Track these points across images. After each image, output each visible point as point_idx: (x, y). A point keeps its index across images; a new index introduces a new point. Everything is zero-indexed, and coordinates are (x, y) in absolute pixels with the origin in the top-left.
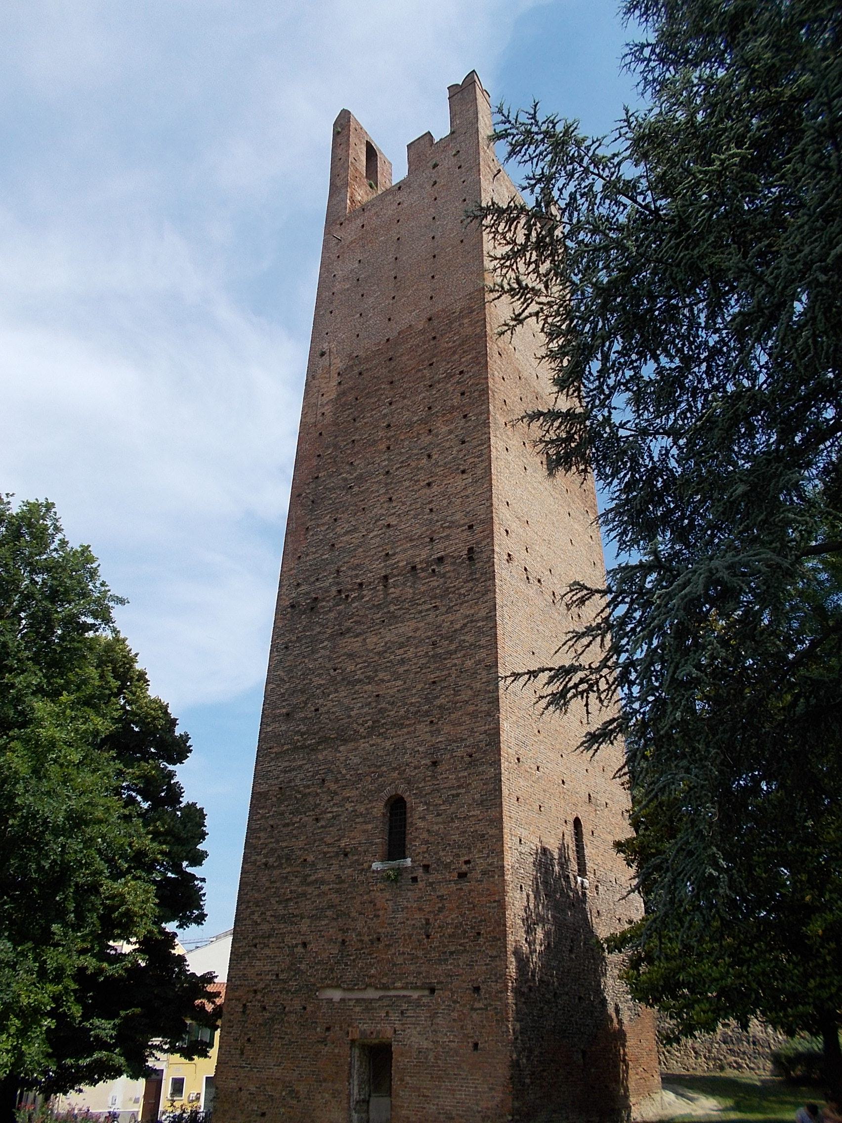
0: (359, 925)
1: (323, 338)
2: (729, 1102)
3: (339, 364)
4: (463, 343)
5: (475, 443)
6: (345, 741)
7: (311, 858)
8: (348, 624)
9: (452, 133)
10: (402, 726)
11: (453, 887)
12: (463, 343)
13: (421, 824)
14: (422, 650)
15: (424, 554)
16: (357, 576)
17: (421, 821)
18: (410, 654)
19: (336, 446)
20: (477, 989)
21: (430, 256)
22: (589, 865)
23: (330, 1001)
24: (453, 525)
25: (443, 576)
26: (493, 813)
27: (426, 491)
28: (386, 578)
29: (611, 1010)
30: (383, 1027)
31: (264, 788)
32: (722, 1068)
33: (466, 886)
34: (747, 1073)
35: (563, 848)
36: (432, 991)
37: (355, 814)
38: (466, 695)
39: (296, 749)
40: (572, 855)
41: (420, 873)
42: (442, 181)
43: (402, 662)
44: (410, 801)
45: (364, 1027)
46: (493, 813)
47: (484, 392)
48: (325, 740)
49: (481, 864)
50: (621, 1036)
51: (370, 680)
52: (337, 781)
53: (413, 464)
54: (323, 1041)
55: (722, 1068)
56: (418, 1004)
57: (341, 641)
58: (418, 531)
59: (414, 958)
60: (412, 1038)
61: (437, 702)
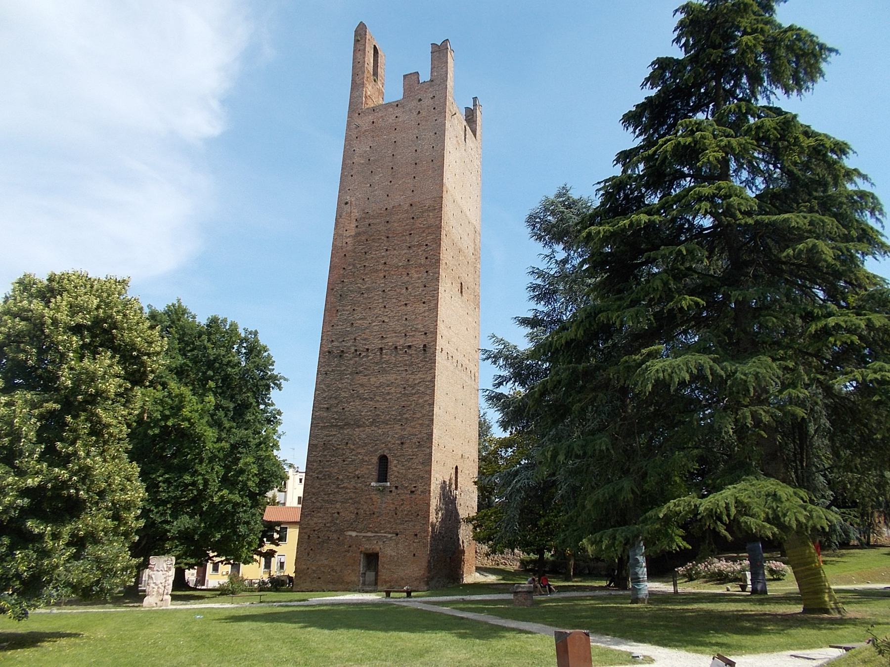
0: (365, 507)
1: (346, 192)
2: (501, 577)
3: (356, 213)
4: (428, 228)
5: (431, 289)
6: (359, 427)
7: (341, 477)
8: (361, 369)
9: (432, 81)
10: (387, 424)
11: (408, 496)
12: (428, 228)
13: (395, 469)
14: (400, 389)
15: (402, 342)
16: (366, 344)
17: (394, 468)
18: (392, 391)
19: (354, 265)
20: (416, 535)
21: (413, 162)
22: (459, 485)
23: (351, 536)
24: (416, 330)
25: (411, 355)
26: (427, 468)
27: (403, 307)
28: (381, 349)
29: (461, 542)
30: (376, 547)
31: (315, 442)
32: (498, 565)
33: (414, 496)
34: (509, 567)
35: (450, 480)
36: (397, 535)
37: (363, 460)
38: (418, 415)
39: (332, 426)
40: (453, 482)
41: (393, 489)
42: (423, 113)
43: (388, 394)
44: (390, 458)
45: (367, 546)
46: (427, 468)
47: (438, 261)
48: (347, 424)
49: (421, 488)
50: (463, 552)
51: (372, 399)
52: (354, 444)
53: (398, 290)
54: (348, 551)
55: (498, 565)
56: (391, 539)
57: (357, 377)
58: (399, 329)
59: (390, 522)
60: (388, 551)
61: (405, 416)
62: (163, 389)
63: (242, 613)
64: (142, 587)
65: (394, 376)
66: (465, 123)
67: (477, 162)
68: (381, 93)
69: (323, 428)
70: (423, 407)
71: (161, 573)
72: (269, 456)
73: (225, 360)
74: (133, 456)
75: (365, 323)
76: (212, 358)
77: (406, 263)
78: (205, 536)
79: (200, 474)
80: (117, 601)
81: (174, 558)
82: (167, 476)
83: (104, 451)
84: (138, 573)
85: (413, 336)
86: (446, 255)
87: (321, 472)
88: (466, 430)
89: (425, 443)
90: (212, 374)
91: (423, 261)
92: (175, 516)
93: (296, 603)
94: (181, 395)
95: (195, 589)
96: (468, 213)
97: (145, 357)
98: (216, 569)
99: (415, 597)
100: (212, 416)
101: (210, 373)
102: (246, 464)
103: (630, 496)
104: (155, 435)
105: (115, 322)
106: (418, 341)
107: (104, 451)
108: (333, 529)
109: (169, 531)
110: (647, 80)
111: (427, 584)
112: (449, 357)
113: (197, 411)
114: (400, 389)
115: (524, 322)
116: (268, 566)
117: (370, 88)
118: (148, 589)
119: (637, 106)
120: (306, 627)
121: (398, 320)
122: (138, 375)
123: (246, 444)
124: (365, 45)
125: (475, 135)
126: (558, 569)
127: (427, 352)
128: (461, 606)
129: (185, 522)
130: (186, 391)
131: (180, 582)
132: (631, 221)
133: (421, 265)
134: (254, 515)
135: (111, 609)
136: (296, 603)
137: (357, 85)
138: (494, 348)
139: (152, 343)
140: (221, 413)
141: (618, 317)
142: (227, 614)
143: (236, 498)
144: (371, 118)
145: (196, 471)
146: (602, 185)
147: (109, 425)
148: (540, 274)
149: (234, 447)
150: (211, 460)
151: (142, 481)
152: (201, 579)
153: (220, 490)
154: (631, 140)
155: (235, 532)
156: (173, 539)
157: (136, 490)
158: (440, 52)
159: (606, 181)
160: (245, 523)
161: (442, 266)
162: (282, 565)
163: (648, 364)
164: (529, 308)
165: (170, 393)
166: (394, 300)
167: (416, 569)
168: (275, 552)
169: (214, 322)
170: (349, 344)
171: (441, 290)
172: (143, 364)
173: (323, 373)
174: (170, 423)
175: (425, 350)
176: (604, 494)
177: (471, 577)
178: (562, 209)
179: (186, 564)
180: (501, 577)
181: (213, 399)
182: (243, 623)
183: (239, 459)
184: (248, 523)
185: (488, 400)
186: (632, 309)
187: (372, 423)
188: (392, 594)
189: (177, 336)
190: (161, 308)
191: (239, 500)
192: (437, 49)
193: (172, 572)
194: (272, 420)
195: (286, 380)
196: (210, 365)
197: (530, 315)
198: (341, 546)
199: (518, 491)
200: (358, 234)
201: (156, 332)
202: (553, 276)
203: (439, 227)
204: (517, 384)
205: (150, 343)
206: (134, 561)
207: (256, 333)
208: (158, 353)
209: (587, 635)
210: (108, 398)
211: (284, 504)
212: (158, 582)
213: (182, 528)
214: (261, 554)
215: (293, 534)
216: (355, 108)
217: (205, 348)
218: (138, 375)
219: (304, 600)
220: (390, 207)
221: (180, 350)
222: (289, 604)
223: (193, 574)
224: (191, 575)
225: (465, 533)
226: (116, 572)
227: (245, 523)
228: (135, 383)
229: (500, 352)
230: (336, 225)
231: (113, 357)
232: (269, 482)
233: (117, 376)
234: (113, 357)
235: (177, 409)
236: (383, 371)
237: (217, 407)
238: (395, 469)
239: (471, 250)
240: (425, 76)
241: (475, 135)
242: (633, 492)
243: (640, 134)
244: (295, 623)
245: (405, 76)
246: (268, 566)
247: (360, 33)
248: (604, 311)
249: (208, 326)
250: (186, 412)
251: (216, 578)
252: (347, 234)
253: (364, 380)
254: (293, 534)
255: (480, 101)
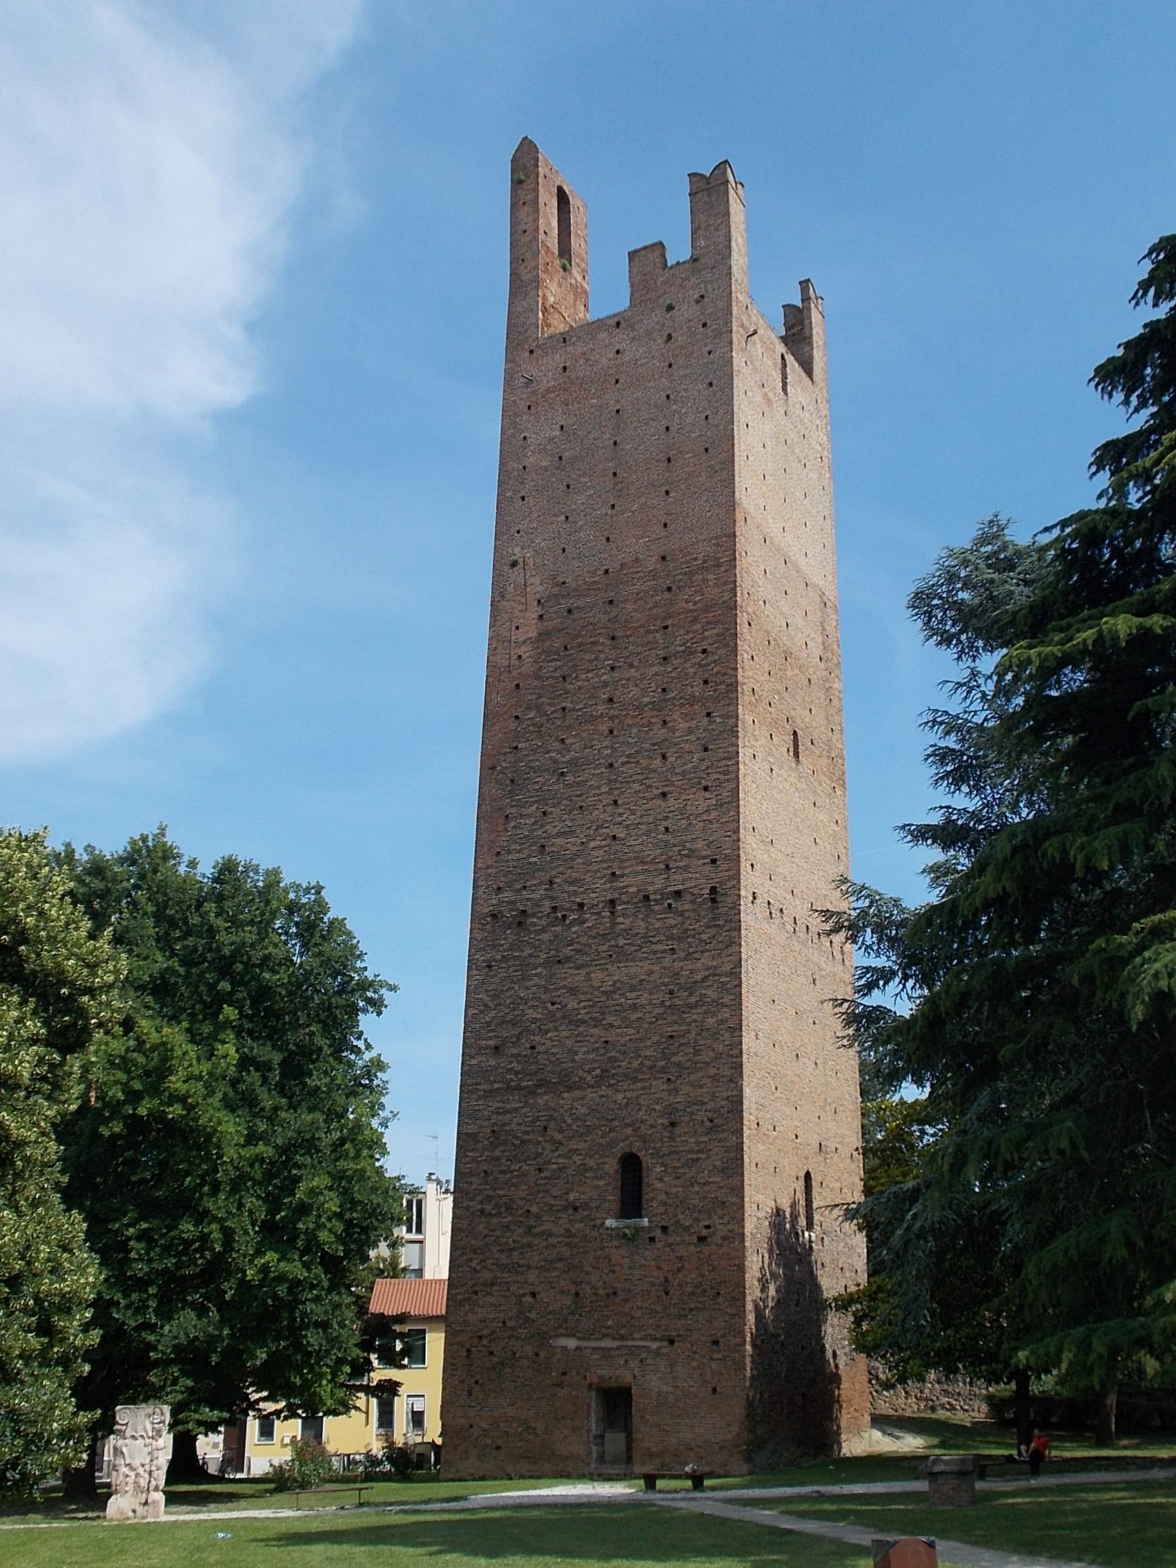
0: (594, 1278)
2: (935, 1441)
3: (537, 588)
4: (707, 609)
6: (570, 1088)
7: (535, 1209)
8: (567, 951)
9: (694, 260)
10: (635, 1080)
11: (692, 1249)
12: (707, 609)
13: (659, 1185)
14: (659, 997)
15: (659, 883)
16: (575, 893)
19: (539, 708)
20: (716, 1342)
23: (565, 1348)
25: (682, 914)
26: (734, 1182)
29: (829, 1354)
31: (473, 1129)
32: (933, 1409)
33: (706, 1249)
34: (960, 1414)
35: (793, 1205)
36: (672, 1342)
37: (585, 1168)
38: (706, 1056)
39: (509, 1089)
40: (802, 1211)
41: (658, 1233)
42: (680, 339)
43: (635, 1007)
44: (646, 1160)
46: (734, 1182)
47: (733, 687)
48: (543, 1083)
49: (721, 1230)
50: (836, 1379)
51: (597, 1022)
52: (561, 1131)
53: (644, 763)
54: (560, 1385)
55: (933, 1409)
56: (657, 1353)
60: (651, 1382)
61: (675, 1059)
62: (126, 1034)
63: (315, 1526)
64: (102, 1478)
65: (646, 964)
66: (781, 348)
67: (819, 438)
68: (580, 294)
69: (489, 1094)
70: (715, 1035)
71: (141, 1444)
72: (363, 1171)
73: (256, 956)
74: (70, 1198)
75: (572, 844)
76: (226, 951)
77: (657, 696)
78: (234, 1355)
79: (215, 1219)
80: (51, 1507)
81: (167, 1409)
82: (144, 1225)
83: (14, 1193)
84: (95, 1440)
85: (686, 868)
86: (752, 671)
87: (489, 1198)
88: (826, 1084)
89: (721, 1123)
90: (228, 987)
91: (697, 691)
92: (166, 1314)
93: (438, 1506)
94: (164, 1044)
95: (219, 1479)
96: (802, 562)
97: (86, 999)
98: (267, 1431)
99: (713, 1489)
100: (234, 1083)
101: (225, 986)
102: (313, 1192)
103: (1124, 1252)
104: (114, 1137)
105: (24, 929)
106: (698, 879)
107: (14, 1193)
108: (523, 1332)
109: (155, 1348)
110: (1144, 286)
111: (749, 1459)
112: (773, 911)
113: (200, 1078)
114: (659, 997)
115: (922, 834)
116: (386, 1419)
117: (553, 287)
118: (116, 1479)
119: (1128, 345)
120: (441, 1552)
121: (648, 833)
122: (72, 1036)
123: (310, 1145)
124: (536, 190)
125: (809, 372)
126: (1078, 1417)
127: (720, 905)
128: (804, 1507)
129: (187, 1325)
130: (175, 1035)
131: (184, 1466)
132: (1100, 632)
133: (693, 701)
134: (337, 1306)
135: (38, 1524)
136: (438, 1506)
137: (522, 285)
138: (848, 906)
139: (96, 965)
140: (253, 1077)
141: (1082, 848)
142: (284, 1528)
143: (295, 1269)
144: (558, 359)
145: (207, 1212)
146: (1056, 532)
147: (23, 1143)
148: (952, 725)
149: (287, 1150)
150: (237, 1185)
151: (91, 1249)
152: (235, 1455)
153: (259, 1253)
154: (1121, 418)
155: (298, 1346)
156: (164, 1363)
157: (81, 1270)
158: (709, 191)
159: (1064, 524)
160: (317, 1325)
161: (744, 699)
162: (417, 1419)
163: (1147, 954)
164: (933, 800)
165: (141, 1043)
166: (636, 787)
167: (721, 1424)
168: (398, 1384)
169: (228, 869)
170: (536, 896)
171: (744, 754)
172: (82, 1013)
173: (482, 966)
174: (142, 1111)
175: (713, 900)
176: (1066, 1252)
177: (862, 1440)
178: (990, 574)
179: (200, 1423)
180: (935, 1441)
181: (232, 1051)
182: (313, 1548)
183: (297, 1180)
184: (325, 1325)
185: (848, 1024)
186: (1113, 830)
187: (601, 1079)
188: (660, 1484)
189: (150, 908)
190: (112, 845)
191: (302, 1274)
192: (703, 185)
193: (166, 1442)
194: (366, 1084)
195: (393, 988)
196: (224, 967)
197: (936, 819)
198: (534, 1370)
199: (921, 1235)
200: (544, 635)
201: (104, 944)
202: (980, 727)
203: (731, 607)
204: (910, 983)
205: (92, 967)
206: (84, 1418)
207: (319, 889)
208: (111, 986)
209: (931, 1545)
210: (18, 1086)
211: (420, 1272)
212: (136, 1463)
213: (183, 1339)
214: (368, 1390)
215: (435, 1343)
216: (521, 338)
217: (212, 931)
218: (72, 1036)
219: (457, 1499)
220: (614, 566)
221: (158, 941)
222: (423, 1507)
223: (215, 1445)
224: (210, 1448)
225: (836, 1332)
226: (49, 1442)
227: (317, 1325)
228: (66, 1050)
229: (864, 913)
230: (493, 616)
231: (24, 1002)
232: (365, 1230)
233: (34, 1040)
234: (24, 1002)
235: (157, 1075)
236: (620, 955)
237: (246, 1062)
238: (659, 1185)
239: (816, 650)
240: (679, 251)
241: (809, 372)
242: (1129, 1244)
243: (1143, 404)
244: (422, 1545)
245: (632, 255)
246: (386, 1419)
247: (525, 165)
248: (1056, 833)
249: (216, 880)
250: (175, 1082)
251: (262, 1457)
252: (521, 636)
253: (578, 978)
254: (435, 1343)
255: (818, 288)
